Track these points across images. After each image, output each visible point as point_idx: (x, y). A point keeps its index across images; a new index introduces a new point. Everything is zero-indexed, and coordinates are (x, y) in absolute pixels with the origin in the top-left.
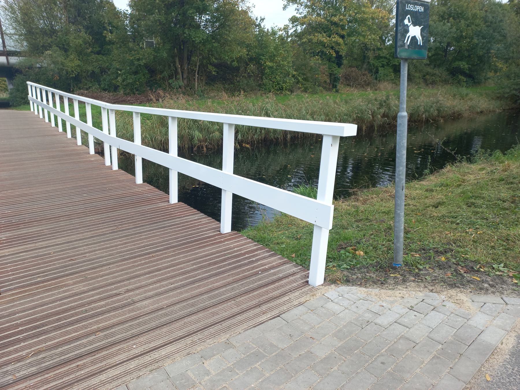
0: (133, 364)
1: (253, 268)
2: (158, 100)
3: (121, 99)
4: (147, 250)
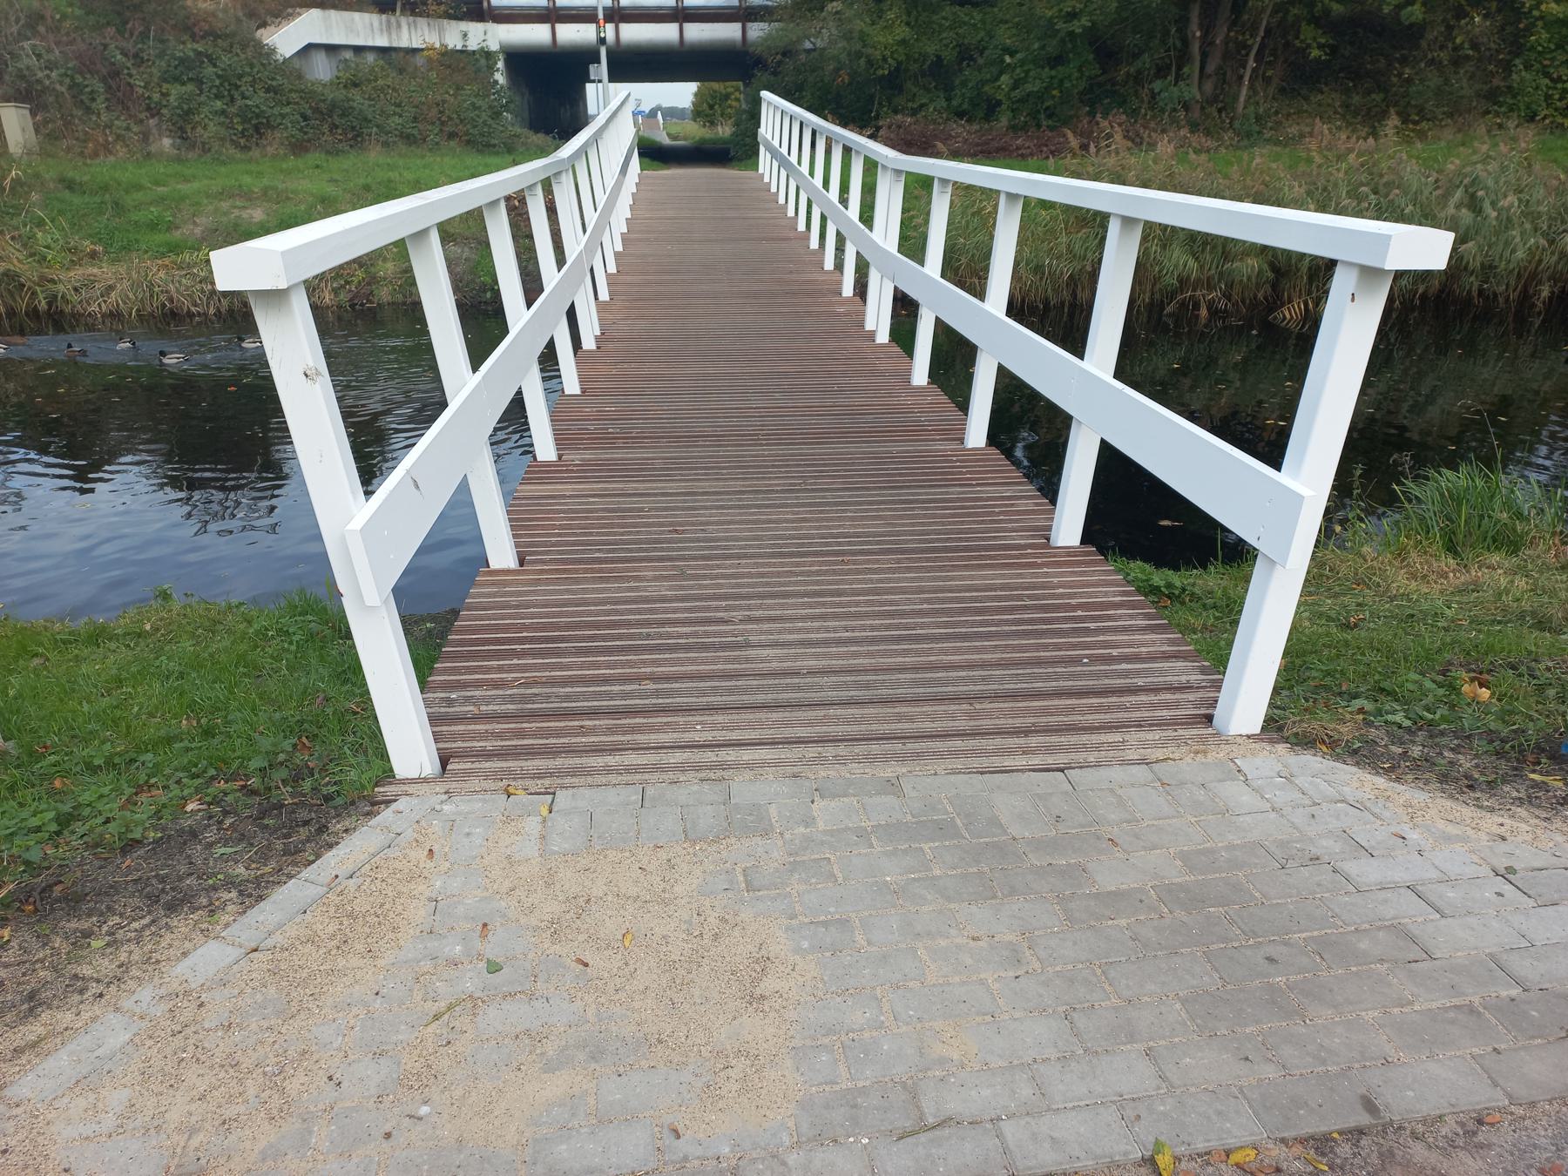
0: (678, 757)
1: (1074, 646)
2: (1085, 147)
3: (995, 144)
4: (839, 544)
